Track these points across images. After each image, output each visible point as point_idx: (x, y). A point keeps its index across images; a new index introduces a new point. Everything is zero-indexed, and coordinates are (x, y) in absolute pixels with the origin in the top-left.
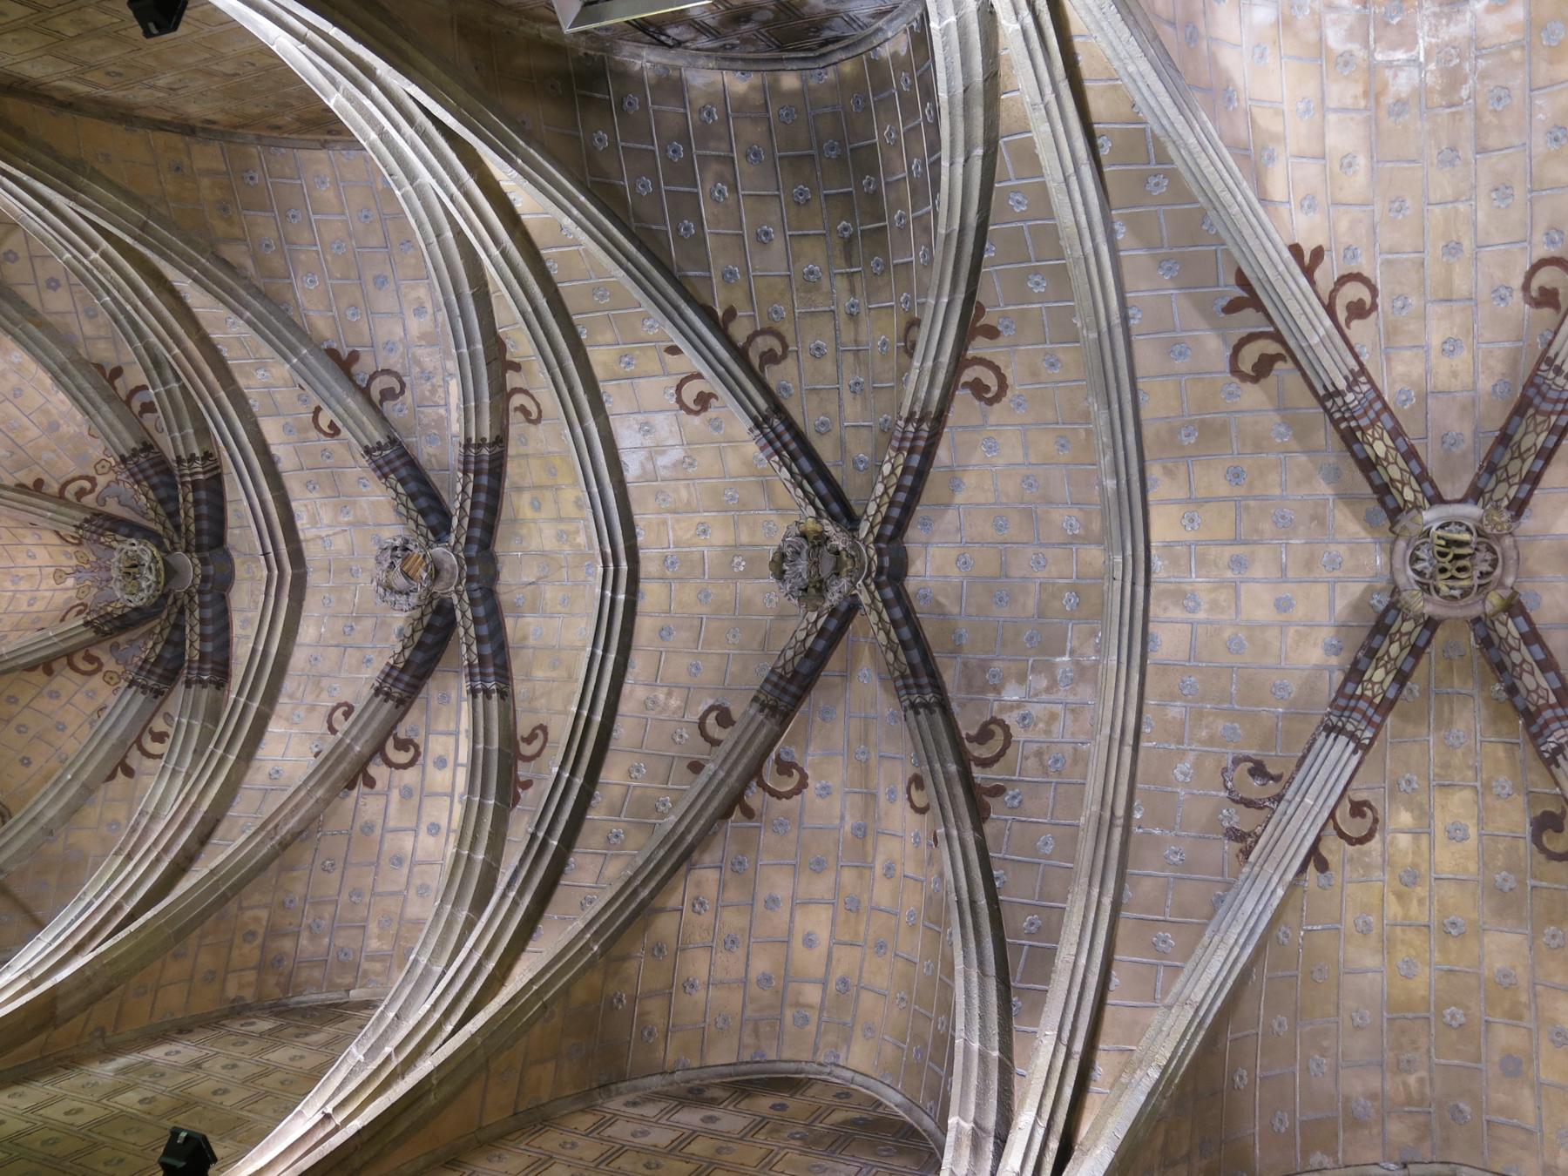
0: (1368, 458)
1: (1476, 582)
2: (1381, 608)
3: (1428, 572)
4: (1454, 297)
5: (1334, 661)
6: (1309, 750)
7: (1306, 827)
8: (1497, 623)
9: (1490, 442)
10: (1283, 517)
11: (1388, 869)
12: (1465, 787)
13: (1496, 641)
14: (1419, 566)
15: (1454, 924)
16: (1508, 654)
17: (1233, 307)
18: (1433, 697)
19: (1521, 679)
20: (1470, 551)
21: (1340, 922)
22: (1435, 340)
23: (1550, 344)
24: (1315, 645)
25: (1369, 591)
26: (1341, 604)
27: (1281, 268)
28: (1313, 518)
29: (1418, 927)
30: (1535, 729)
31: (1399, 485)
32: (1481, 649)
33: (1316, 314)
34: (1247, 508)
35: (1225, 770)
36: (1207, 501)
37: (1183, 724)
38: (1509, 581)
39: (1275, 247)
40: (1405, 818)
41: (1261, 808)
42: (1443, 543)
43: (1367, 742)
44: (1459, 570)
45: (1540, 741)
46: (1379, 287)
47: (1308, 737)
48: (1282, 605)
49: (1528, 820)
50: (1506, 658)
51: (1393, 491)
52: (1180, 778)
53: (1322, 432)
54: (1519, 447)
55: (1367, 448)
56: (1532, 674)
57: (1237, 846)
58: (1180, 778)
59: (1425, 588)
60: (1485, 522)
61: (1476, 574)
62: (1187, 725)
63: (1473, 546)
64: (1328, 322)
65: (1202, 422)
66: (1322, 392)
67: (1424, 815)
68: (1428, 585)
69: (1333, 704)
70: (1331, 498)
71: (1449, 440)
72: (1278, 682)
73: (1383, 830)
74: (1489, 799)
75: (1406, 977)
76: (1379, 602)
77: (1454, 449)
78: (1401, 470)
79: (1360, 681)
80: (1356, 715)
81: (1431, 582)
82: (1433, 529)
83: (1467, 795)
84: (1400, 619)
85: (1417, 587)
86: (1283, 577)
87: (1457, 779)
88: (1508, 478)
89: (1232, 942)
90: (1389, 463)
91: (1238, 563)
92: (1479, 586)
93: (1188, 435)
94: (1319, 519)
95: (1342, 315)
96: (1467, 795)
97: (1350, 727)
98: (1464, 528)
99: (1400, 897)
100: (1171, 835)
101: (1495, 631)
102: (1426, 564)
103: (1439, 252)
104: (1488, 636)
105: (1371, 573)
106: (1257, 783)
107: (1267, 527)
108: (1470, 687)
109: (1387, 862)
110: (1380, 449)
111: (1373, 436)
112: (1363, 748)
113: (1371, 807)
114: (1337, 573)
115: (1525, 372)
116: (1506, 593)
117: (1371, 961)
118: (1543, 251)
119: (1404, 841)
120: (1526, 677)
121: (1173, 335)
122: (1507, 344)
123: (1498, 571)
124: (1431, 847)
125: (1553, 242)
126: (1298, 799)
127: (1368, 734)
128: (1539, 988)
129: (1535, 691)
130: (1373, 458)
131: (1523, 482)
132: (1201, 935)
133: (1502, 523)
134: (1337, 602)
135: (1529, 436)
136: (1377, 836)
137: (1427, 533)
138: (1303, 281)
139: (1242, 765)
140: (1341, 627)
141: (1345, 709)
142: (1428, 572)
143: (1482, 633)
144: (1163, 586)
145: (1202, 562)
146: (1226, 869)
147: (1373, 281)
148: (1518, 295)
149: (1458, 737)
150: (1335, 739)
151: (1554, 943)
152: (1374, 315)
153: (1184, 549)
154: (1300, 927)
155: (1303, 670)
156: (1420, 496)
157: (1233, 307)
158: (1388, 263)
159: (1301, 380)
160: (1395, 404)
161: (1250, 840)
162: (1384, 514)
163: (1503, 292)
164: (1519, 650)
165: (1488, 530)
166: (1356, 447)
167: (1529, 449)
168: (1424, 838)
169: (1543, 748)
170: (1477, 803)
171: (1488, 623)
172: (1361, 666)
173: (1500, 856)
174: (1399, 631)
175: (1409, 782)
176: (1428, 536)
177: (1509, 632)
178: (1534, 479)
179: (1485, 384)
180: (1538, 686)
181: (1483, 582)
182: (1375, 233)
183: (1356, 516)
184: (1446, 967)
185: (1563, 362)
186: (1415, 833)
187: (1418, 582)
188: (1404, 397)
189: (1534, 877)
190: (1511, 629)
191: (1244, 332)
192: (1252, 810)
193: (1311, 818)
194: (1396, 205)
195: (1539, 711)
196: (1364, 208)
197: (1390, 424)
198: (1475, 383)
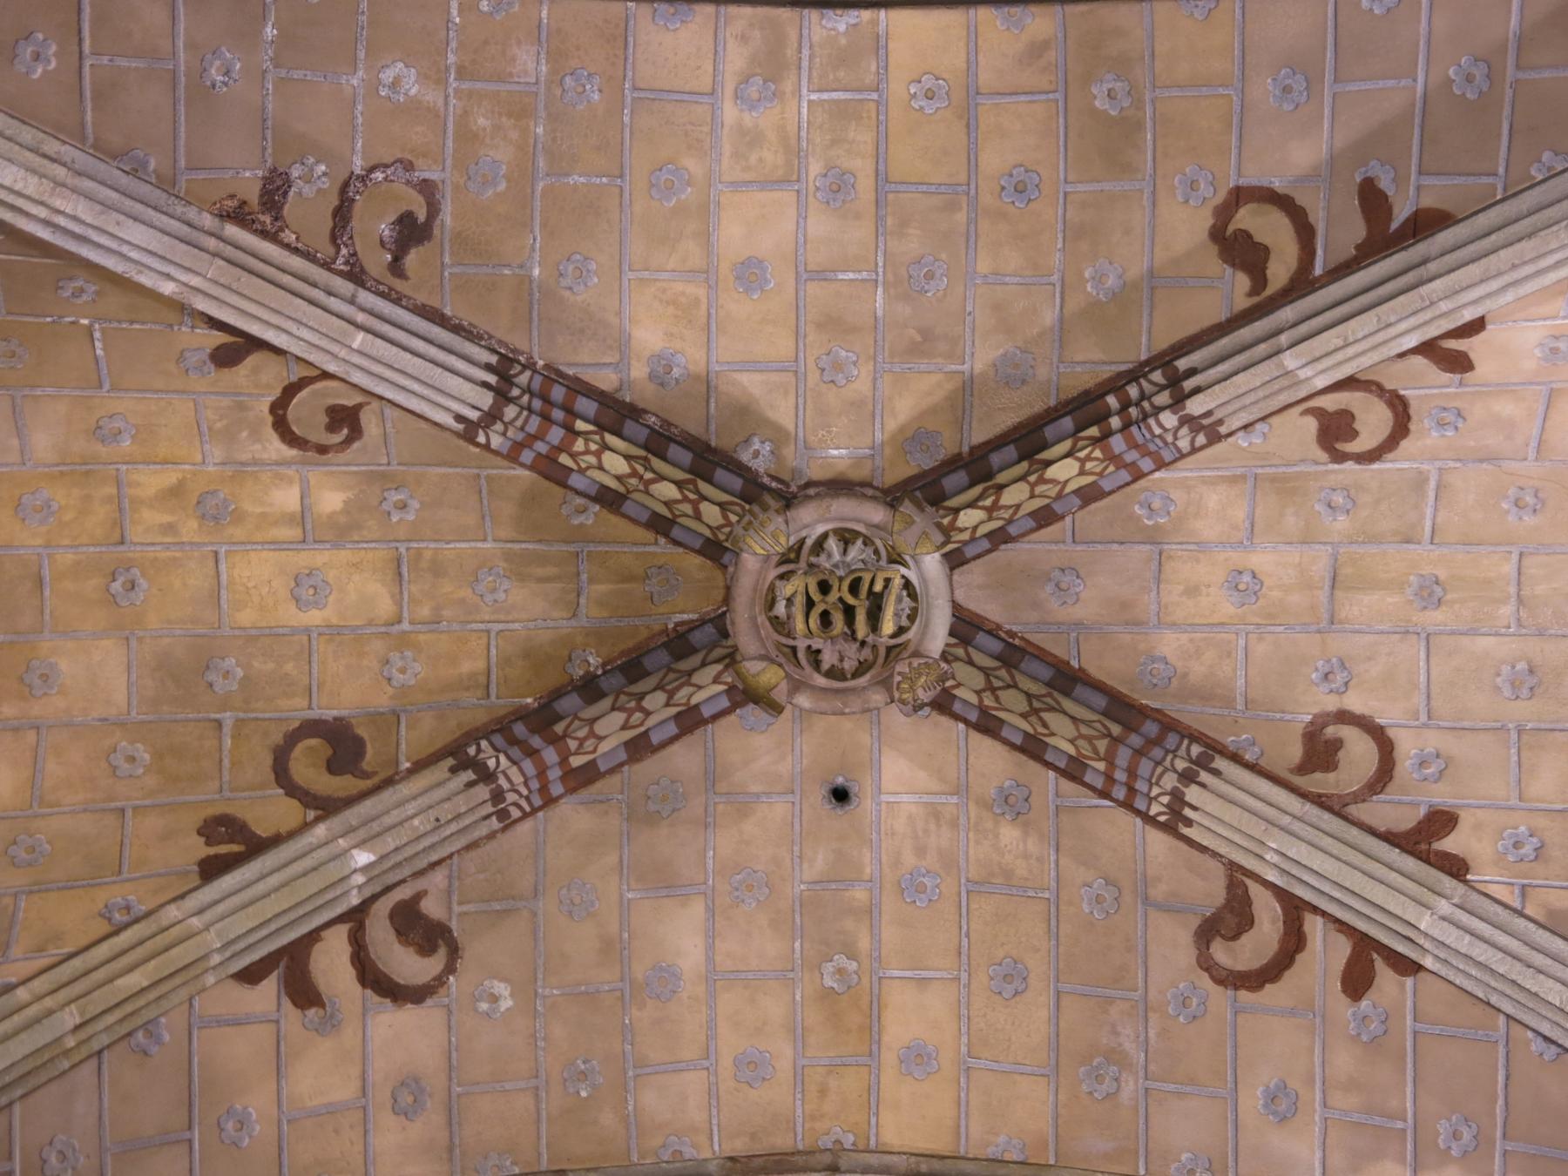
0: (1045, 446)
1: (801, 644)
2: (745, 457)
3: (822, 560)
4: (1339, 594)
5: (639, 371)
6: (457, 329)
7: (305, 333)
8: (719, 667)
9: (1059, 651)
10: (930, 276)
11: (229, 470)
12: (399, 604)
13: (684, 665)
14: (832, 544)
15: (132, 586)
16: (659, 687)
17: (1372, 199)
18: (572, 548)
19: (613, 709)
20: (860, 634)
21: (113, 389)
22: (1261, 560)
23: (1236, 758)
24: (669, 335)
25: (779, 436)
26: (752, 384)
27: (1444, 306)
28: (927, 335)
29: (119, 523)
30: (519, 729)
31: (988, 502)
32: (665, 631)
33: (1340, 364)
34: (951, 207)
35: (409, 166)
36: (970, 127)
37: (500, 78)
38: (803, 700)
39: (1489, 295)
40: (331, 501)
41: (334, 238)
42: (878, 587)
43: (481, 439)
44: (825, 618)
45: (498, 739)
46: (1376, 466)
47: (482, 324)
48: (750, 274)
49: (344, 713)
50: (651, 682)
51: (977, 490)
52: (388, 76)
53: (1098, 355)
54: (1051, 709)
55: (1066, 445)
56: (624, 728)
57: (253, 195)
58: (388, 76)
59: (791, 557)
60: (916, 662)
61: (817, 644)
62: (503, 87)
63: (870, 639)
64: (1321, 382)
65: (1140, 125)
66: (1182, 364)
67: (340, 532)
68: (797, 560)
69: (553, 374)
70: (966, 367)
71: (1066, 579)
72: (593, 266)
73: (304, 463)
74: (378, 646)
75: (18, 506)
76: (756, 454)
77: (1049, 588)
78: (1018, 507)
79: (602, 427)
80: (534, 424)
81: (803, 564)
82: (903, 570)
83: (384, 606)
84: (725, 497)
85: (792, 540)
86: (807, 274)
87: (414, 588)
88: (993, 690)
89: (58, 203)
90: (1033, 486)
91: (838, 186)
92: (794, 649)
93: (1111, 95)
94: (923, 345)
95: (1330, 402)
96: (384, 606)
97: (510, 412)
98: (904, 622)
99: (175, 493)
100: (266, 57)
101: (704, 664)
102: (837, 557)
103: (1427, 570)
104: (694, 651)
105: (812, 439)
106: (385, 229)
107: (912, 244)
108: (590, 612)
109: (241, 471)
110: (1064, 470)
111: (1088, 458)
112: (469, 431)
113: (348, 441)
114: (813, 377)
115: (1190, 714)
116: (780, 695)
117: (43, 443)
118: (1407, 746)
119: (287, 498)
120: (618, 718)
121: (1329, 77)
122: (1241, 682)
123: (821, 681)
124: (277, 545)
125: (1423, 764)
126: (361, 317)
127: (496, 441)
128: (31, 736)
129: (592, 734)
130: (1045, 455)
131: (983, 711)
132: (56, 130)
133: (912, 689)
134: (757, 377)
135: (1072, 727)
136: (292, 453)
137: (896, 559)
138: (1411, 341)
139: (421, 199)
140: (707, 384)
141: (546, 400)
142: (822, 560)
143: (697, 637)
144: (793, 35)
145: (842, 113)
146: (202, 175)
147: (1390, 456)
148: (1331, 704)
149: (494, 590)
150: (485, 385)
151: (118, 759)
152: (1323, 456)
153: (870, 79)
154: (97, 319)
155: (619, 313)
156: (966, 536)
157: (1372, 199)
158: (1420, 481)
159: (1207, 322)
160: (1146, 489)
161: (267, 219)
162: (928, 464)
163: (1340, 678)
164: (667, 705)
165: (902, 667)
166: (1067, 423)
167: (1045, 725)
168: (293, 533)
169: (484, 744)
170: (370, 623)
171: (718, 652)
172: (630, 427)
173: (271, 666)
174: (704, 498)
175: (403, 506)
176: (891, 561)
177: (700, 687)
178: (988, 725)
179: (1169, 645)
180: (601, 739)
181: (801, 655)
182: (1481, 461)
183: (932, 411)
184: (46, 573)
185: (1203, 785)
186: (302, 518)
187: (802, 542)
188: (1157, 504)
189: (240, 723)
190: (707, 689)
191: (1318, 218)
192: (330, 224)
193: (324, 343)
194: (1530, 500)
195: (556, 740)
196: (1534, 444)
197: (1106, 485)
198: (1173, 625)
